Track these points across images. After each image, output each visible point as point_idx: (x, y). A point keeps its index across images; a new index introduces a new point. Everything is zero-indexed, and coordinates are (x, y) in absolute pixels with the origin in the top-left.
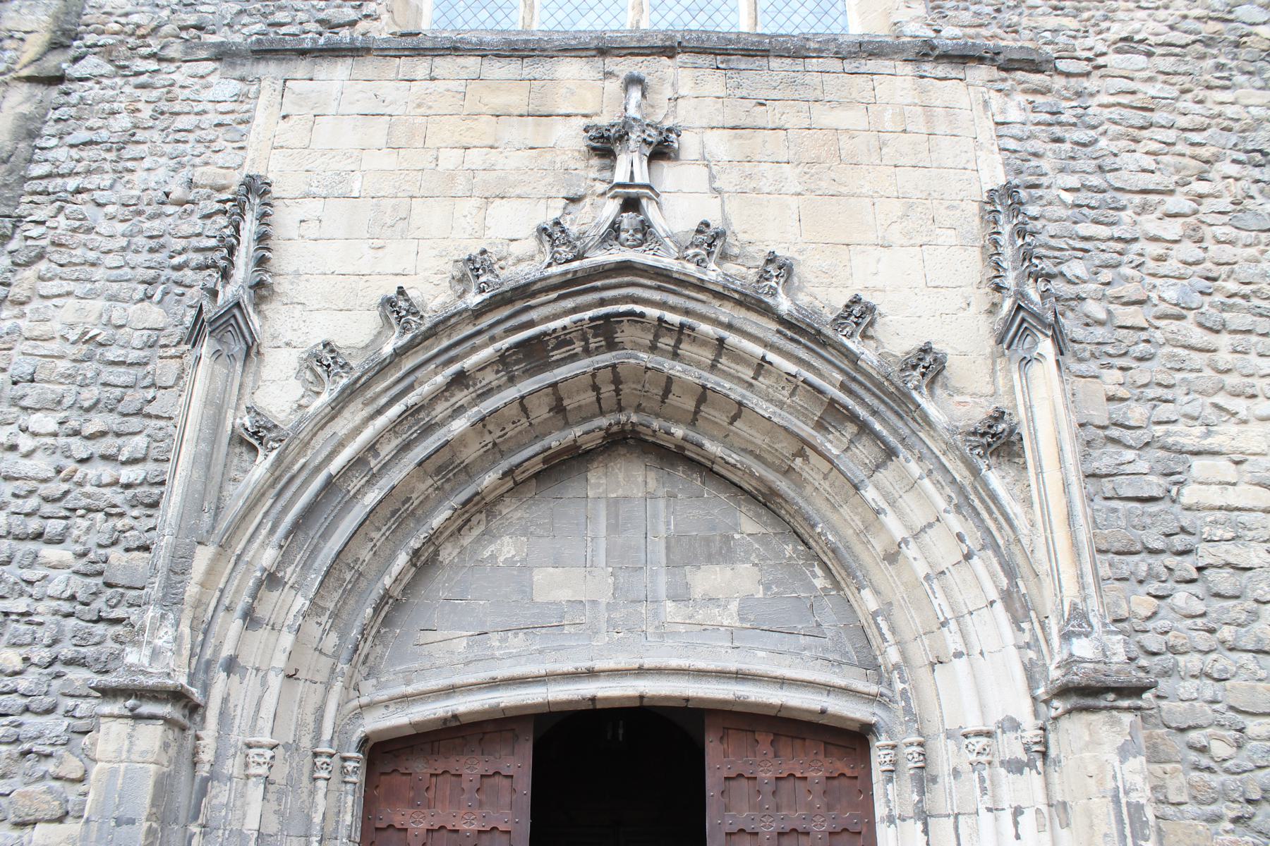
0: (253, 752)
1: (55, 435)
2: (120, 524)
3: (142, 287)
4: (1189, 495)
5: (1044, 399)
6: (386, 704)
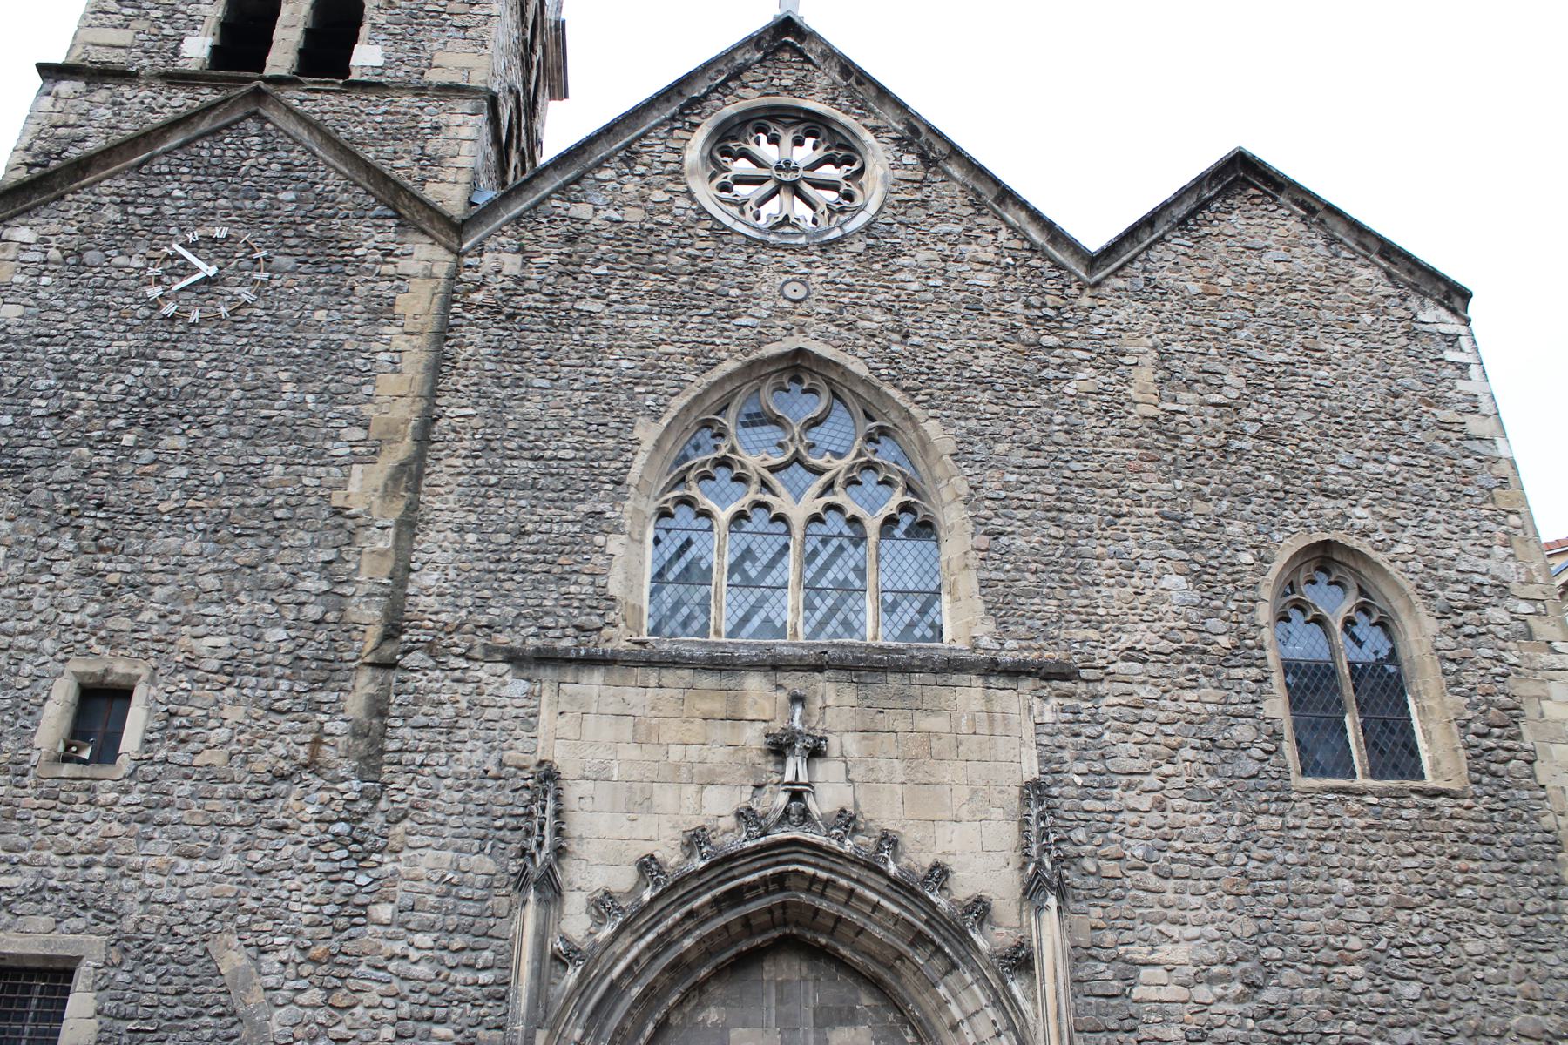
2: (483, 1011)
3: (477, 843)
4: (1137, 993)
5: (1049, 936)
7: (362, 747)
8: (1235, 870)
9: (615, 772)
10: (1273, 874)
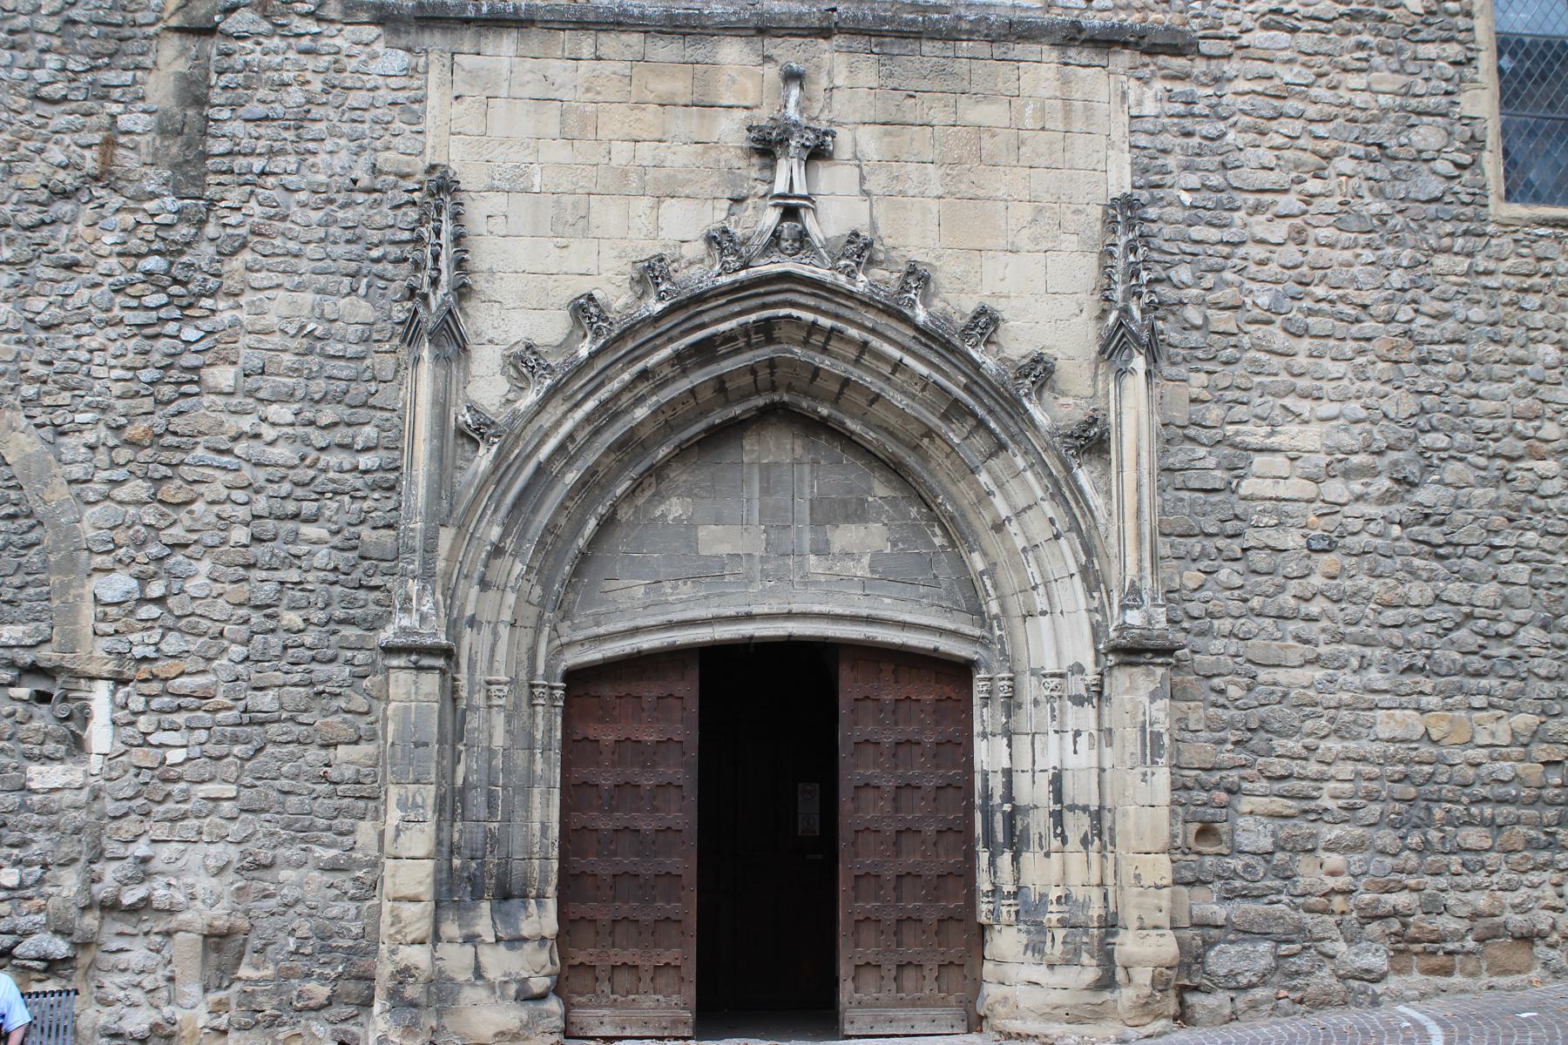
0: (493, 688)
1: (292, 425)
2: (366, 505)
3: (347, 280)
4: (1247, 487)
5: (1133, 410)
6: (582, 643)
7: (174, 150)
8: (1396, 328)
9: (537, 180)
10: (1448, 336)
